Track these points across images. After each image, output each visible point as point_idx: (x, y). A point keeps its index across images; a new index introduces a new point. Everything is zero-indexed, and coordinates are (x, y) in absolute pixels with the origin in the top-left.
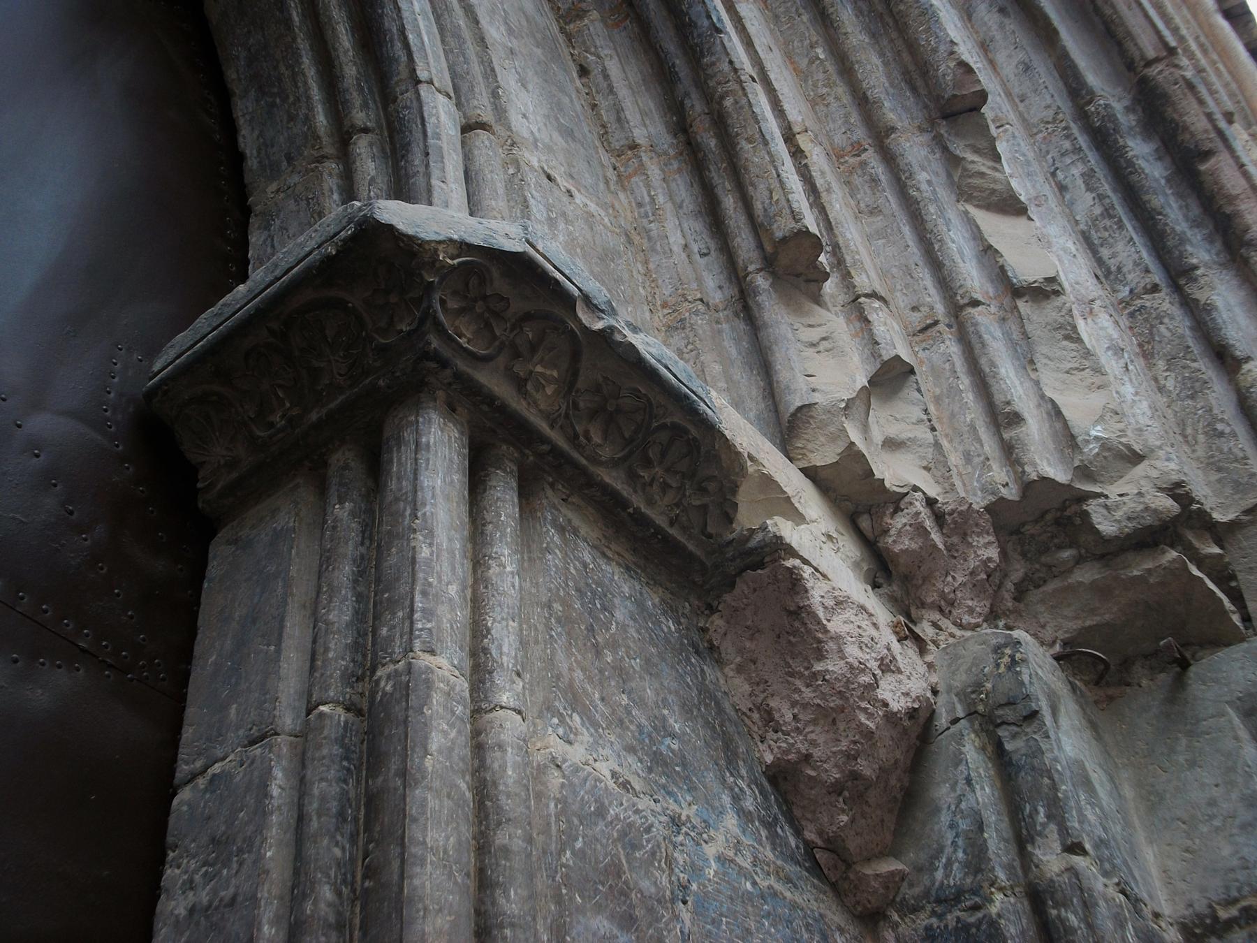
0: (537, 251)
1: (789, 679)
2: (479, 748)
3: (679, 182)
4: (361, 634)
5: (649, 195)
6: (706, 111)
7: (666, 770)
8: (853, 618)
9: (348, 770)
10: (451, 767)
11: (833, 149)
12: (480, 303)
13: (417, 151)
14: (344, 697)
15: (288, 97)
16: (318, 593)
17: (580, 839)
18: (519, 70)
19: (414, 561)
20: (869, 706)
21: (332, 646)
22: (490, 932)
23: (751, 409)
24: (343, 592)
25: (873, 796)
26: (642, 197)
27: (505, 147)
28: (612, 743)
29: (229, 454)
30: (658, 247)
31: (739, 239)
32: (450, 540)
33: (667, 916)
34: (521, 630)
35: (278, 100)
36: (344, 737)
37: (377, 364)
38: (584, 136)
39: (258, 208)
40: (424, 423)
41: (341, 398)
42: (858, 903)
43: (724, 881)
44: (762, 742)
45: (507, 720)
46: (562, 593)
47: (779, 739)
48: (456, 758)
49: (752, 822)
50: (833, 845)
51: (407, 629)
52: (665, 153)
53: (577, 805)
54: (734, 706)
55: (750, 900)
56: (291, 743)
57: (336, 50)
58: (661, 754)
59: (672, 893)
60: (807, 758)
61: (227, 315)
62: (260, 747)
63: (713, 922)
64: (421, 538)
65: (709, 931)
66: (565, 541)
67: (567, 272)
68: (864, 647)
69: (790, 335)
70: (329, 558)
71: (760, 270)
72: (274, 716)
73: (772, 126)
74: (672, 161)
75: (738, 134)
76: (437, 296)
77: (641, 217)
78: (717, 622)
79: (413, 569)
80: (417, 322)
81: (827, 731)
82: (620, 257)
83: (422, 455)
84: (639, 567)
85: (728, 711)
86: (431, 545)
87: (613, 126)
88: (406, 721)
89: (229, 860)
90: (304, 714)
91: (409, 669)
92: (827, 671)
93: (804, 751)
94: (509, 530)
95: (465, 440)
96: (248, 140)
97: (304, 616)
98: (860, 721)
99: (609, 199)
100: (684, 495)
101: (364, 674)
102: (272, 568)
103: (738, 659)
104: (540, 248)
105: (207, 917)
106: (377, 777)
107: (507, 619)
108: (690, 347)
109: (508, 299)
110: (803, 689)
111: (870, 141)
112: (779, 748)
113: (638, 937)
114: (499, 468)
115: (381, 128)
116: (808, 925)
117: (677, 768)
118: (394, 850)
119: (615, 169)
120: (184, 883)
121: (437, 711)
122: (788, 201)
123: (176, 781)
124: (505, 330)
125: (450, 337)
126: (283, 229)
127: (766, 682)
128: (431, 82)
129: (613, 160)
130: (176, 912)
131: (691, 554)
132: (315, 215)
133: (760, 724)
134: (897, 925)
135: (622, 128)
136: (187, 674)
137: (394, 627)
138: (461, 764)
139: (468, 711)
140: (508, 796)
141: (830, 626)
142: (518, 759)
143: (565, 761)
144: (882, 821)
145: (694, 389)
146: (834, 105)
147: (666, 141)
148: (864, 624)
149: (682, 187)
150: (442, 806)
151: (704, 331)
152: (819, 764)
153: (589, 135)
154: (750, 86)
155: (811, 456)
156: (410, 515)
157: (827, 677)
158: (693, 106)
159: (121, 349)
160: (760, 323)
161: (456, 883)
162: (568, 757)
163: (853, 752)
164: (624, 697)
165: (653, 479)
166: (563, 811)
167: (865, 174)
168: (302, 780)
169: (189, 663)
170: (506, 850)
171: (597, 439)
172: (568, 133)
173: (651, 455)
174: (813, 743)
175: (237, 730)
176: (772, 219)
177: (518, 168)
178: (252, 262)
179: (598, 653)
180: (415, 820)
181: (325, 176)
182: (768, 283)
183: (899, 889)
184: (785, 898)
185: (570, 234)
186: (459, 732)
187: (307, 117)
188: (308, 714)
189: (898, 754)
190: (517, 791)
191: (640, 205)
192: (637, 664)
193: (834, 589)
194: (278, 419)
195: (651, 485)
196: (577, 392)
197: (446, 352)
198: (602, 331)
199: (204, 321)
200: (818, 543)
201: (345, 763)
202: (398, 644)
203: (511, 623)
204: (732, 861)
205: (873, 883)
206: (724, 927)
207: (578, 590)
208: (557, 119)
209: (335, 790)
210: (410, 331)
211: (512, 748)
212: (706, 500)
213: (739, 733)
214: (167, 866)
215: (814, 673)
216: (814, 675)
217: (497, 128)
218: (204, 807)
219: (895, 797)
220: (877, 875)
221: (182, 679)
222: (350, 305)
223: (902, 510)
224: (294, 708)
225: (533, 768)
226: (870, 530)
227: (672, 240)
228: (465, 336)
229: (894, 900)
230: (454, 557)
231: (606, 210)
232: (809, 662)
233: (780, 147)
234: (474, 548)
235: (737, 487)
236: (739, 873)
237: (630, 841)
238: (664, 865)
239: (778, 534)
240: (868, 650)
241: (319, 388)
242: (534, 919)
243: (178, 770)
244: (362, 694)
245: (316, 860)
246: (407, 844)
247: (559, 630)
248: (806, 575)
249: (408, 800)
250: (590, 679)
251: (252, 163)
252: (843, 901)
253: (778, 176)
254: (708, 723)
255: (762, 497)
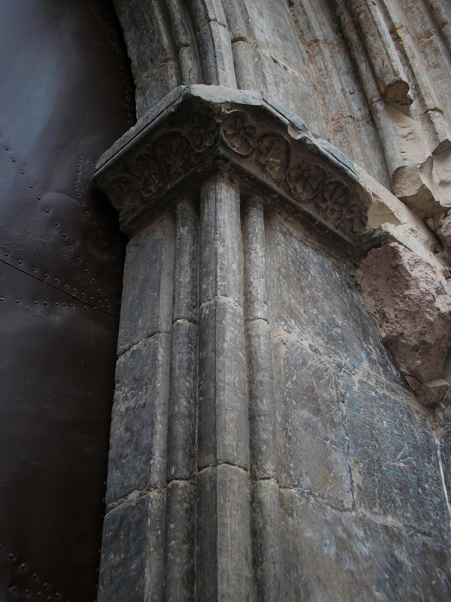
0: (268, 104)
1: (393, 298)
2: (248, 337)
3: (339, 57)
4: (194, 287)
5: (324, 65)
6: (351, 21)
7: (335, 343)
8: (423, 269)
9: (191, 348)
10: (236, 346)
11: (416, 35)
12: (242, 130)
13: (210, 55)
14: (188, 316)
15: (149, 30)
16: (175, 268)
17: (295, 376)
18: (259, 7)
19: (216, 254)
20: (430, 310)
21: (182, 293)
22: (255, 418)
23: (375, 169)
24: (186, 268)
25: (433, 351)
26: (321, 66)
27: (253, 48)
28: (309, 332)
29: (132, 205)
30: (329, 91)
31: (368, 85)
32: (232, 243)
33: (335, 409)
34: (266, 282)
35: (145, 32)
36: (188, 333)
37: (196, 162)
38: (292, 38)
39: (139, 86)
40: (219, 189)
41: (181, 178)
42: (426, 400)
43: (362, 392)
44: (380, 327)
45: (260, 324)
46: (285, 264)
47: (388, 326)
48: (238, 343)
49: (376, 364)
50: (414, 374)
51: (214, 285)
52: (332, 43)
53: (293, 361)
54: (367, 311)
55: (375, 400)
56: (166, 336)
57: (170, 6)
58: (333, 335)
59: (338, 398)
60: (402, 334)
61: (127, 142)
62: (153, 338)
63: (357, 410)
64: (219, 243)
65: (355, 415)
66: (286, 239)
67: (283, 113)
68: (428, 283)
69: (393, 132)
70: (179, 253)
71: (378, 101)
72: (158, 325)
73: (384, 28)
74: (336, 47)
75: (367, 33)
76: (222, 130)
77: (320, 76)
78: (359, 272)
79: (216, 258)
80: (213, 142)
81: (411, 322)
82: (311, 97)
83: (219, 204)
84: (321, 248)
85: (364, 314)
86: (224, 246)
87: (306, 31)
88: (215, 327)
89: (142, 387)
90: (171, 323)
91: (216, 304)
92: (411, 294)
93: (400, 332)
94: (259, 236)
95: (238, 195)
96: (132, 52)
97: (169, 279)
98: (426, 317)
99: (305, 68)
100: (342, 214)
101: (196, 305)
102: (154, 257)
103: (369, 289)
104: (269, 102)
105: (133, 412)
106: (203, 352)
107: (259, 278)
108: (345, 140)
109: (255, 128)
110: (400, 303)
111: (434, 30)
112: (388, 330)
113: (321, 419)
114: (255, 207)
115: (194, 43)
116: (401, 411)
117: (340, 342)
118: (212, 384)
119: (307, 53)
120: (123, 397)
121: (229, 322)
122: (392, 66)
123: (118, 353)
124: (255, 142)
125: (229, 147)
126: (151, 95)
127: (383, 300)
128: (216, 20)
129: (306, 48)
130: (121, 410)
131: (346, 241)
132: (165, 88)
133: (380, 319)
134: (444, 410)
135: (310, 32)
136: (120, 305)
137: (209, 284)
138: (240, 345)
139: (243, 321)
140: (262, 358)
141: (412, 273)
142: (266, 341)
143: (287, 341)
144: (438, 362)
145: (346, 164)
146: (416, 12)
147: (332, 37)
148: (428, 272)
149: (340, 60)
150: (232, 364)
151: (352, 132)
152: (407, 337)
153: (294, 37)
154: (372, 7)
155: (404, 191)
156: (214, 232)
157: (411, 297)
158: (345, 19)
159: (81, 159)
160: (378, 127)
161: (239, 398)
162: (289, 339)
163: (423, 332)
164: (315, 310)
165: (327, 208)
166: (287, 364)
167: (432, 47)
168: (171, 353)
169: (121, 300)
170: (261, 382)
171: (300, 190)
172: (284, 37)
173: (326, 196)
174: (404, 328)
175: (142, 330)
176: (384, 75)
177: (260, 58)
178: (137, 112)
179: (303, 291)
180: (220, 371)
181: (169, 68)
182: (383, 107)
183: (445, 393)
184: (391, 399)
185: (286, 89)
186: (239, 331)
187: (158, 40)
188: (173, 324)
189: (445, 332)
190: (266, 356)
191: (320, 70)
192: (321, 294)
193: (414, 256)
194: (153, 189)
195: (326, 210)
196: (290, 169)
197: (227, 155)
198: (300, 140)
199: (117, 144)
200: (407, 234)
201: (190, 345)
202: (211, 292)
203: (262, 279)
204: (365, 383)
205: (433, 391)
206: (362, 413)
207: (292, 262)
208: (278, 30)
209: (185, 357)
210: (210, 146)
211: (263, 337)
212: (353, 216)
213: (369, 324)
214: (116, 390)
215: (405, 296)
216: (405, 297)
217: (249, 39)
218: (130, 365)
219: (444, 352)
220: (435, 387)
221: (118, 308)
222: (182, 135)
223: (449, 216)
224: (167, 321)
225: (273, 345)
226: (433, 225)
227: (336, 87)
228: (236, 147)
229: (442, 398)
230: (234, 251)
231: (303, 74)
232: (402, 290)
233: (388, 38)
234: (244, 245)
235: (367, 209)
236: (369, 388)
237: (318, 376)
238: (334, 386)
239: (387, 231)
240: (430, 284)
241: (171, 173)
242: (274, 412)
243: (118, 348)
244: (196, 314)
245: (179, 388)
246: (217, 382)
247: (284, 281)
248: (400, 250)
249: (217, 362)
250: (299, 303)
251: (135, 63)
252: (419, 399)
253: (387, 53)
254: (355, 320)
255: (380, 213)
